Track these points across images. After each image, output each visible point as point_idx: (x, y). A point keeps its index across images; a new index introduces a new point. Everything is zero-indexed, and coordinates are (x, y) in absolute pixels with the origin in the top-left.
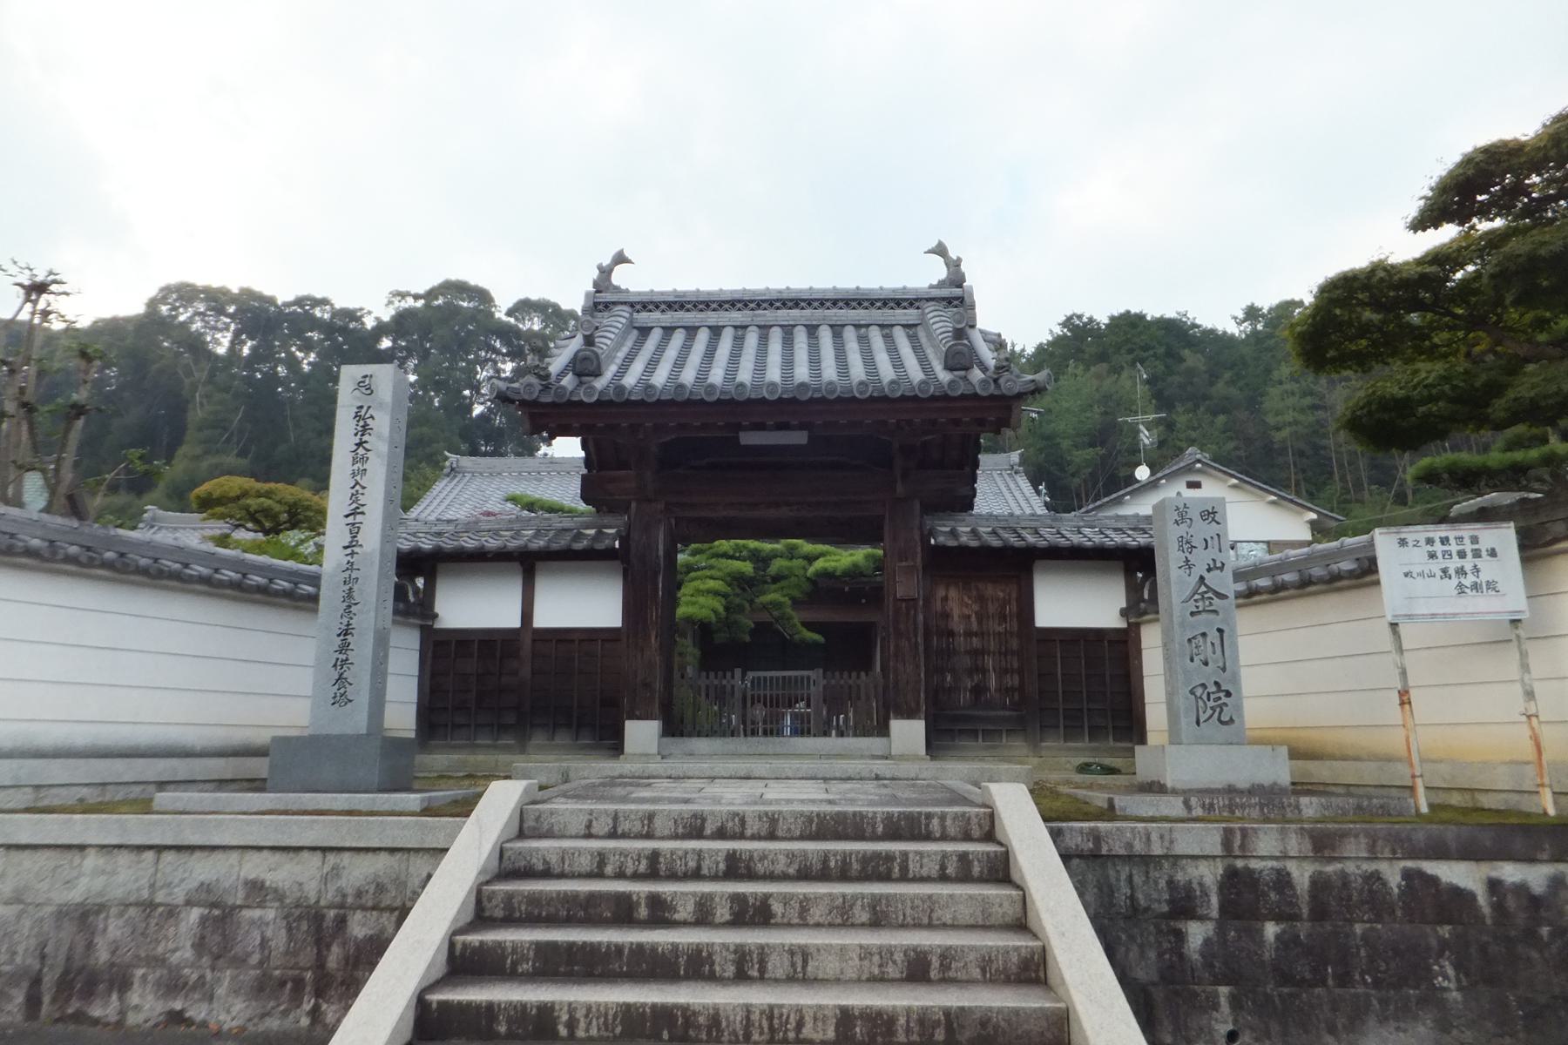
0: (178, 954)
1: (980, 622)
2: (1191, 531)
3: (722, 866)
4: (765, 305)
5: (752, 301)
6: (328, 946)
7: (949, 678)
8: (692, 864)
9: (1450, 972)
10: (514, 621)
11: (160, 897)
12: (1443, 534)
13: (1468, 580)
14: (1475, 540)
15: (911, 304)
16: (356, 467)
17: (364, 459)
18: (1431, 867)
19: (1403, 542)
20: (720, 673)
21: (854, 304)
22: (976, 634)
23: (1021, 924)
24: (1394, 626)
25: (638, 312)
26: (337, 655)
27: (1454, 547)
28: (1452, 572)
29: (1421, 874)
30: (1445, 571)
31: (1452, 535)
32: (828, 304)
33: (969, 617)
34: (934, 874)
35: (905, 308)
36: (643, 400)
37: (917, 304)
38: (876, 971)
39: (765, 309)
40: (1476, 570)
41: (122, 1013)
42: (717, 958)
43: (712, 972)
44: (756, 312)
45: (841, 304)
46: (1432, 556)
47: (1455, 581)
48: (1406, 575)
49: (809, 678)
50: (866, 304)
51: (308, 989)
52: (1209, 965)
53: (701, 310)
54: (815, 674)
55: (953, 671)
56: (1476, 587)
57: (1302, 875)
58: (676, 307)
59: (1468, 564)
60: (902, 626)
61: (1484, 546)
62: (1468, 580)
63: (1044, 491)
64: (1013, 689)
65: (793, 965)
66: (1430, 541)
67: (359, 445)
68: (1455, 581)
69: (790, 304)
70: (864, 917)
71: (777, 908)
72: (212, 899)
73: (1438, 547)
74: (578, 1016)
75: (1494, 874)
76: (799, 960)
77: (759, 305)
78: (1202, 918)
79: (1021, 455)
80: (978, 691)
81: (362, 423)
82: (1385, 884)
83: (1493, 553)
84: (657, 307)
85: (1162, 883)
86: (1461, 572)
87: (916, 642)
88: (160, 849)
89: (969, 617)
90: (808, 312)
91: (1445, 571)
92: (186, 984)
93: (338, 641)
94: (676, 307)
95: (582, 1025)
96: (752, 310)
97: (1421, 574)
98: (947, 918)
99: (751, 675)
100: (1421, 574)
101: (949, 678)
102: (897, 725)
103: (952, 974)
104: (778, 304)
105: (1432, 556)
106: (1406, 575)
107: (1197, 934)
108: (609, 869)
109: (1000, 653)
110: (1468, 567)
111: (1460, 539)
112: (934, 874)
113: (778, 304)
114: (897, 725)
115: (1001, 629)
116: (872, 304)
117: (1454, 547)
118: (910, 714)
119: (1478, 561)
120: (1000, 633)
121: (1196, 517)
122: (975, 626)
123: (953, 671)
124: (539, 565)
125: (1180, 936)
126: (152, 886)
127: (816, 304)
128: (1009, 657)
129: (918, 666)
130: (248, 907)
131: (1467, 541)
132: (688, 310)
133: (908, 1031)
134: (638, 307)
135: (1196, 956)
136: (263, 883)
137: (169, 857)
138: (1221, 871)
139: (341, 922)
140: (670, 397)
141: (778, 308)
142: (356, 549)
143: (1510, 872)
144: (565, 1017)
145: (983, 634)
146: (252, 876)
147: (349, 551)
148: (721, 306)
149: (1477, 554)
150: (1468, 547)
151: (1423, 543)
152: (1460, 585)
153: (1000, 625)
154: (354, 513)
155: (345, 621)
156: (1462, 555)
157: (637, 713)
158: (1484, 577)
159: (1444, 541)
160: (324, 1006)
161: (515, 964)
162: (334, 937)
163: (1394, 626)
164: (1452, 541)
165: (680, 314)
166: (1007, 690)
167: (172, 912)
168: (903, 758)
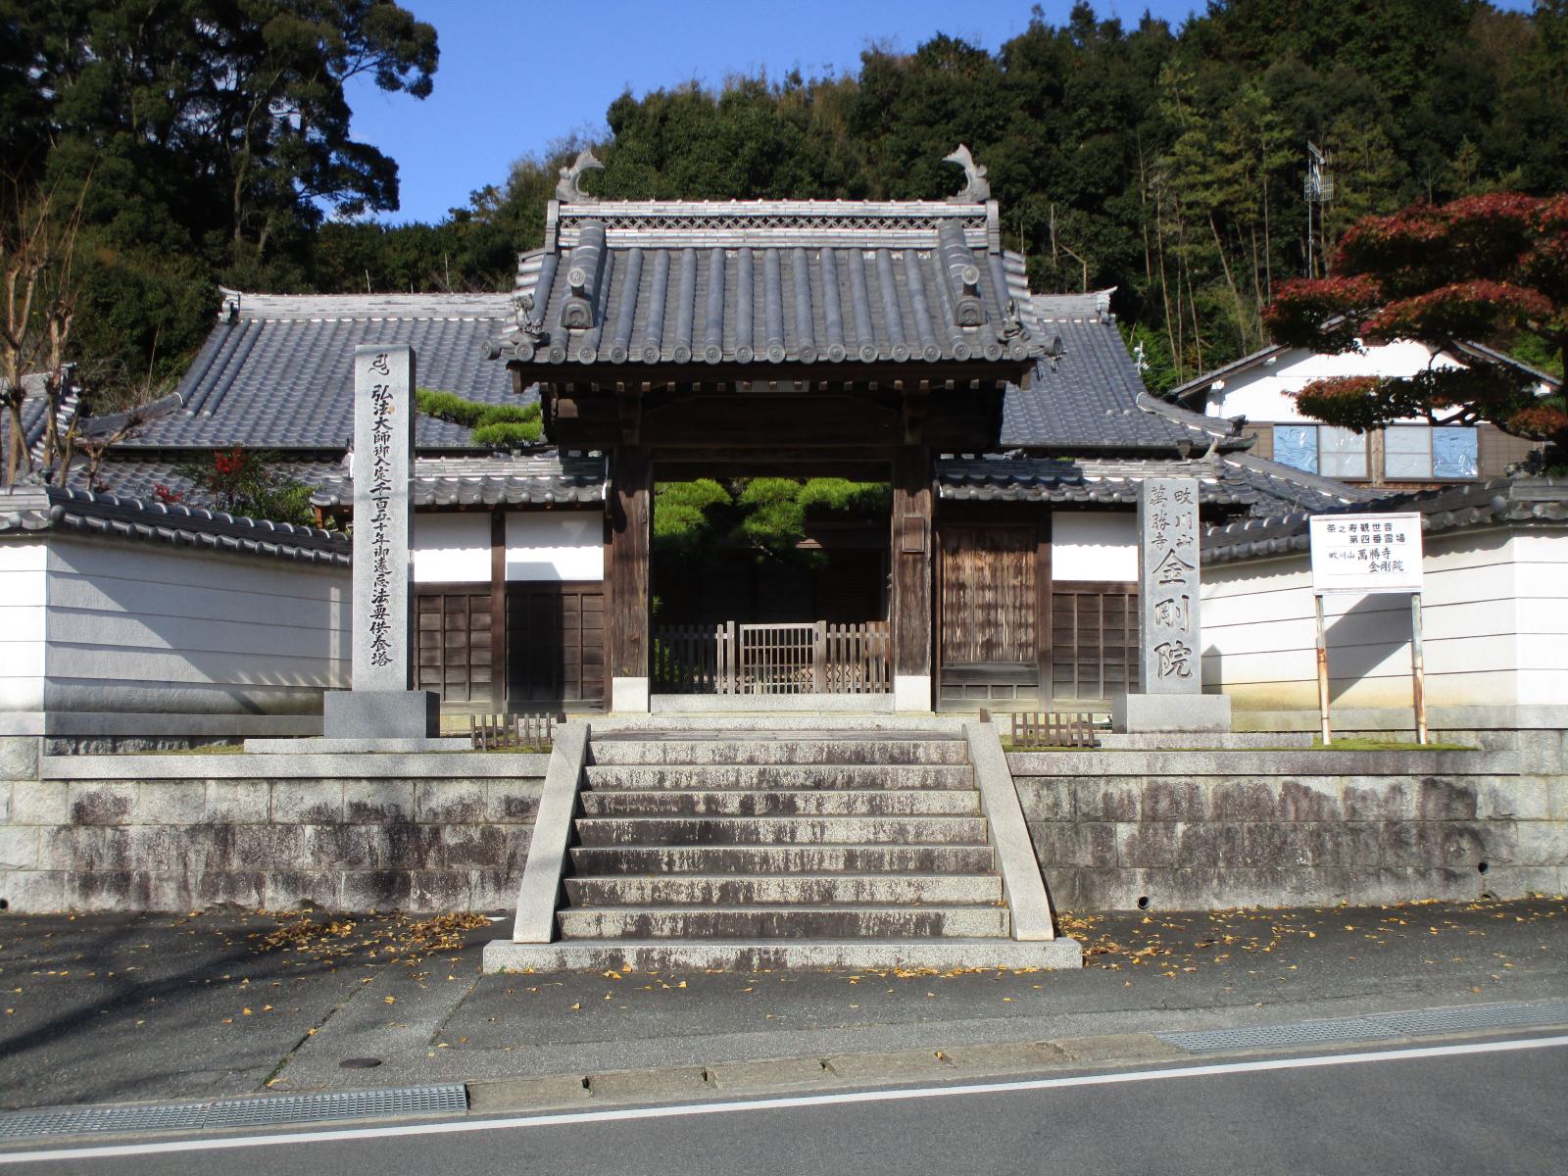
0: (300, 860)
1: (994, 575)
2: (1166, 510)
3: (755, 780)
4: (758, 222)
5: (742, 217)
6: (426, 852)
7: (958, 633)
8: (732, 779)
9: (1309, 854)
10: (486, 576)
11: (278, 817)
12: (1364, 522)
13: (1379, 562)
14: (1388, 527)
15: (926, 222)
16: (378, 445)
17: (386, 438)
18: (1304, 782)
19: (1331, 528)
20: (701, 627)
21: (861, 221)
22: (989, 588)
23: (980, 812)
24: (1319, 597)
25: (611, 227)
26: (373, 620)
27: (1371, 533)
28: (1367, 553)
29: (1297, 786)
30: (1362, 552)
31: (1382, 522)
32: (831, 221)
33: (982, 569)
34: (917, 784)
35: (919, 227)
36: (642, 362)
37: (933, 223)
38: (872, 837)
39: (758, 227)
40: (1387, 552)
41: (261, 903)
42: (761, 830)
43: (758, 840)
44: (748, 231)
45: (845, 221)
46: (1354, 540)
47: (1369, 561)
48: (1331, 555)
49: (810, 631)
50: (874, 222)
51: (413, 883)
52: (1130, 854)
53: (684, 227)
54: (819, 627)
55: (964, 625)
56: (1385, 566)
57: (1208, 789)
58: (655, 222)
59: (1381, 547)
60: (908, 580)
61: (1394, 532)
62: (1379, 562)
63: (1142, 355)
64: (1027, 645)
65: (814, 834)
66: (1353, 528)
67: (380, 423)
68: (1369, 561)
69: (788, 221)
70: (864, 809)
71: (800, 803)
72: (323, 819)
73: (1359, 533)
74: (1283, 245)
75: (1351, 785)
76: (818, 830)
77: (751, 222)
78: (1130, 821)
79: (1113, 296)
80: (989, 646)
81: (380, 402)
82: (1269, 793)
83: (1402, 538)
84: (633, 222)
85: (1100, 796)
86: (1375, 553)
87: (923, 598)
88: (272, 781)
89: (982, 569)
90: (807, 231)
91: (1362, 552)
92: (311, 881)
93: (374, 606)
94: (655, 222)
95: (678, 863)
96: (744, 227)
97: (1344, 555)
98: (924, 809)
99: (744, 627)
100: (1344, 555)
101: (958, 633)
102: (901, 681)
103: (924, 838)
104: (773, 221)
105: (1354, 540)
106: (1331, 555)
107: (1124, 832)
108: (667, 784)
109: (1014, 607)
110: (1381, 550)
111: (1377, 526)
112: (917, 784)
113: (773, 221)
114: (901, 681)
115: (1016, 582)
116: (882, 222)
117: (1371, 533)
118: (916, 670)
119: (1389, 545)
120: (1014, 587)
121: (1171, 497)
122: (988, 580)
123: (964, 625)
124: (508, 515)
125: (1111, 834)
126: (270, 809)
127: (817, 221)
128: (1024, 612)
129: (924, 622)
130: (354, 824)
131: (1382, 528)
132: (669, 227)
133: (891, 863)
134: (611, 222)
135: (1123, 849)
136: (365, 805)
137: (281, 787)
138: (1145, 786)
139: (436, 832)
140: (670, 359)
141: (773, 226)
142: (384, 522)
143: (1363, 784)
144: (666, 859)
145: (996, 587)
146: (355, 801)
147: (377, 524)
148: (707, 222)
149: (1389, 539)
150: (1383, 533)
151: (1347, 529)
152: (1373, 565)
153: (1016, 577)
154: (380, 487)
155: (379, 588)
156: (1377, 539)
157: (626, 670)
158: (1392, 558)
159: (1364, 527)
160: (429, 896)
161: (619, 837)
162: (430, 845)
163: (1319, 597)
164: (1371, 528)
165: (661, 232)
166: (1021, 646)
167: (289, 828)
168: (905, 713)
